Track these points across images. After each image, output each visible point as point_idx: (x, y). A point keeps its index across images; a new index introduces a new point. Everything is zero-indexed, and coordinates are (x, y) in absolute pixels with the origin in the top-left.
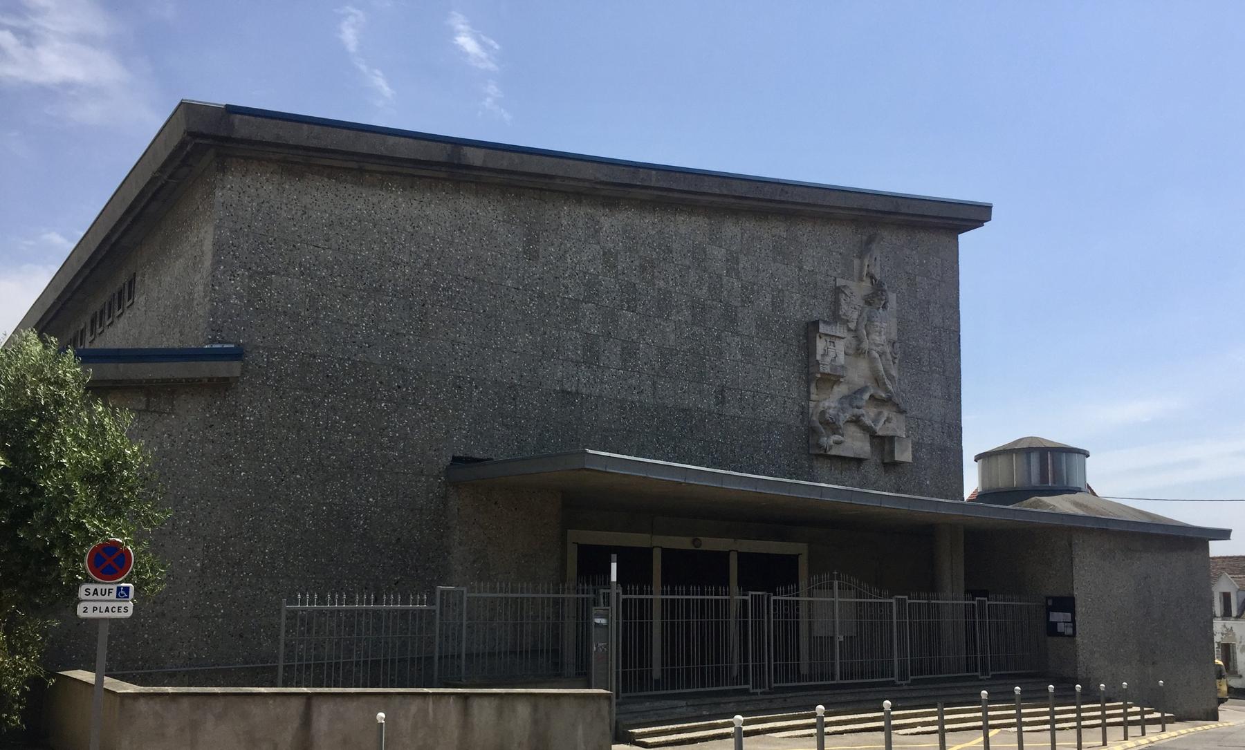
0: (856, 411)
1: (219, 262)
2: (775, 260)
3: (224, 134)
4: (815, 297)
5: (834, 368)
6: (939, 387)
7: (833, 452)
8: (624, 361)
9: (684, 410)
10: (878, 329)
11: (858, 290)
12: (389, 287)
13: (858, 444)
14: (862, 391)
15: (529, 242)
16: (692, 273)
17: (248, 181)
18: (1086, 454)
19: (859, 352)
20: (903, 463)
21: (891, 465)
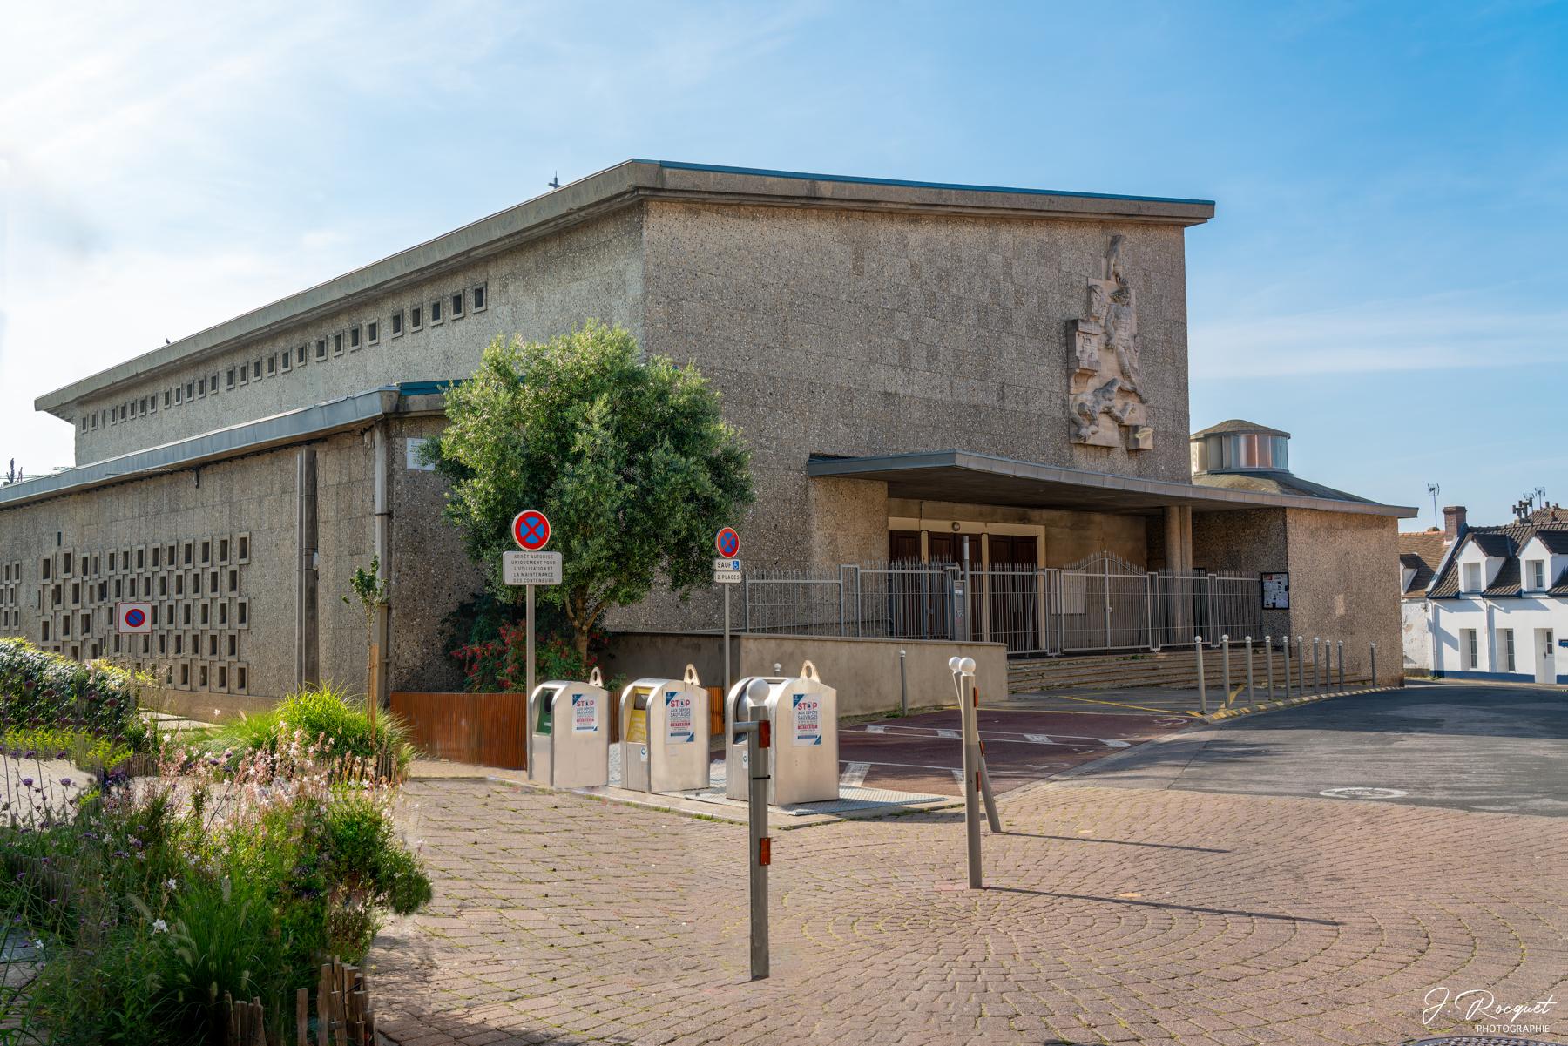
0: (1108, 402)
1: (648, 292)
2: (1039, 264)
3: (660, 186)
4: (1072, 296)
5: (1090, 363)
6: (1170, 378)
7: (1089, 442)
8: (929, 363)
9: (974, 406)
10: (1124, 325)
11: (1107, 287)
12: (760, 306)
13: (1109, 433)
14: (1112, 383)
15: (856, 260)
16: (977, 279)
17: (664, 220)
18: (1288, 436)
19: (1108, 346)
20: (1144, 450)
21: (1134, 451)
